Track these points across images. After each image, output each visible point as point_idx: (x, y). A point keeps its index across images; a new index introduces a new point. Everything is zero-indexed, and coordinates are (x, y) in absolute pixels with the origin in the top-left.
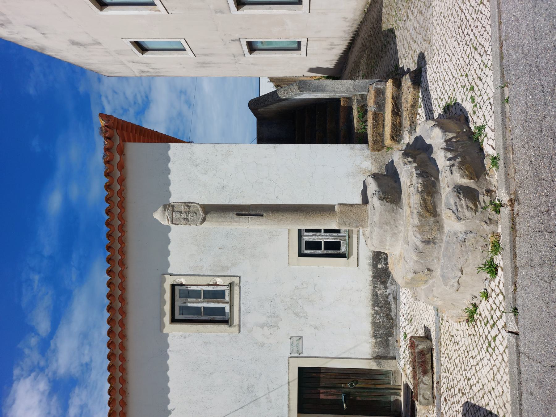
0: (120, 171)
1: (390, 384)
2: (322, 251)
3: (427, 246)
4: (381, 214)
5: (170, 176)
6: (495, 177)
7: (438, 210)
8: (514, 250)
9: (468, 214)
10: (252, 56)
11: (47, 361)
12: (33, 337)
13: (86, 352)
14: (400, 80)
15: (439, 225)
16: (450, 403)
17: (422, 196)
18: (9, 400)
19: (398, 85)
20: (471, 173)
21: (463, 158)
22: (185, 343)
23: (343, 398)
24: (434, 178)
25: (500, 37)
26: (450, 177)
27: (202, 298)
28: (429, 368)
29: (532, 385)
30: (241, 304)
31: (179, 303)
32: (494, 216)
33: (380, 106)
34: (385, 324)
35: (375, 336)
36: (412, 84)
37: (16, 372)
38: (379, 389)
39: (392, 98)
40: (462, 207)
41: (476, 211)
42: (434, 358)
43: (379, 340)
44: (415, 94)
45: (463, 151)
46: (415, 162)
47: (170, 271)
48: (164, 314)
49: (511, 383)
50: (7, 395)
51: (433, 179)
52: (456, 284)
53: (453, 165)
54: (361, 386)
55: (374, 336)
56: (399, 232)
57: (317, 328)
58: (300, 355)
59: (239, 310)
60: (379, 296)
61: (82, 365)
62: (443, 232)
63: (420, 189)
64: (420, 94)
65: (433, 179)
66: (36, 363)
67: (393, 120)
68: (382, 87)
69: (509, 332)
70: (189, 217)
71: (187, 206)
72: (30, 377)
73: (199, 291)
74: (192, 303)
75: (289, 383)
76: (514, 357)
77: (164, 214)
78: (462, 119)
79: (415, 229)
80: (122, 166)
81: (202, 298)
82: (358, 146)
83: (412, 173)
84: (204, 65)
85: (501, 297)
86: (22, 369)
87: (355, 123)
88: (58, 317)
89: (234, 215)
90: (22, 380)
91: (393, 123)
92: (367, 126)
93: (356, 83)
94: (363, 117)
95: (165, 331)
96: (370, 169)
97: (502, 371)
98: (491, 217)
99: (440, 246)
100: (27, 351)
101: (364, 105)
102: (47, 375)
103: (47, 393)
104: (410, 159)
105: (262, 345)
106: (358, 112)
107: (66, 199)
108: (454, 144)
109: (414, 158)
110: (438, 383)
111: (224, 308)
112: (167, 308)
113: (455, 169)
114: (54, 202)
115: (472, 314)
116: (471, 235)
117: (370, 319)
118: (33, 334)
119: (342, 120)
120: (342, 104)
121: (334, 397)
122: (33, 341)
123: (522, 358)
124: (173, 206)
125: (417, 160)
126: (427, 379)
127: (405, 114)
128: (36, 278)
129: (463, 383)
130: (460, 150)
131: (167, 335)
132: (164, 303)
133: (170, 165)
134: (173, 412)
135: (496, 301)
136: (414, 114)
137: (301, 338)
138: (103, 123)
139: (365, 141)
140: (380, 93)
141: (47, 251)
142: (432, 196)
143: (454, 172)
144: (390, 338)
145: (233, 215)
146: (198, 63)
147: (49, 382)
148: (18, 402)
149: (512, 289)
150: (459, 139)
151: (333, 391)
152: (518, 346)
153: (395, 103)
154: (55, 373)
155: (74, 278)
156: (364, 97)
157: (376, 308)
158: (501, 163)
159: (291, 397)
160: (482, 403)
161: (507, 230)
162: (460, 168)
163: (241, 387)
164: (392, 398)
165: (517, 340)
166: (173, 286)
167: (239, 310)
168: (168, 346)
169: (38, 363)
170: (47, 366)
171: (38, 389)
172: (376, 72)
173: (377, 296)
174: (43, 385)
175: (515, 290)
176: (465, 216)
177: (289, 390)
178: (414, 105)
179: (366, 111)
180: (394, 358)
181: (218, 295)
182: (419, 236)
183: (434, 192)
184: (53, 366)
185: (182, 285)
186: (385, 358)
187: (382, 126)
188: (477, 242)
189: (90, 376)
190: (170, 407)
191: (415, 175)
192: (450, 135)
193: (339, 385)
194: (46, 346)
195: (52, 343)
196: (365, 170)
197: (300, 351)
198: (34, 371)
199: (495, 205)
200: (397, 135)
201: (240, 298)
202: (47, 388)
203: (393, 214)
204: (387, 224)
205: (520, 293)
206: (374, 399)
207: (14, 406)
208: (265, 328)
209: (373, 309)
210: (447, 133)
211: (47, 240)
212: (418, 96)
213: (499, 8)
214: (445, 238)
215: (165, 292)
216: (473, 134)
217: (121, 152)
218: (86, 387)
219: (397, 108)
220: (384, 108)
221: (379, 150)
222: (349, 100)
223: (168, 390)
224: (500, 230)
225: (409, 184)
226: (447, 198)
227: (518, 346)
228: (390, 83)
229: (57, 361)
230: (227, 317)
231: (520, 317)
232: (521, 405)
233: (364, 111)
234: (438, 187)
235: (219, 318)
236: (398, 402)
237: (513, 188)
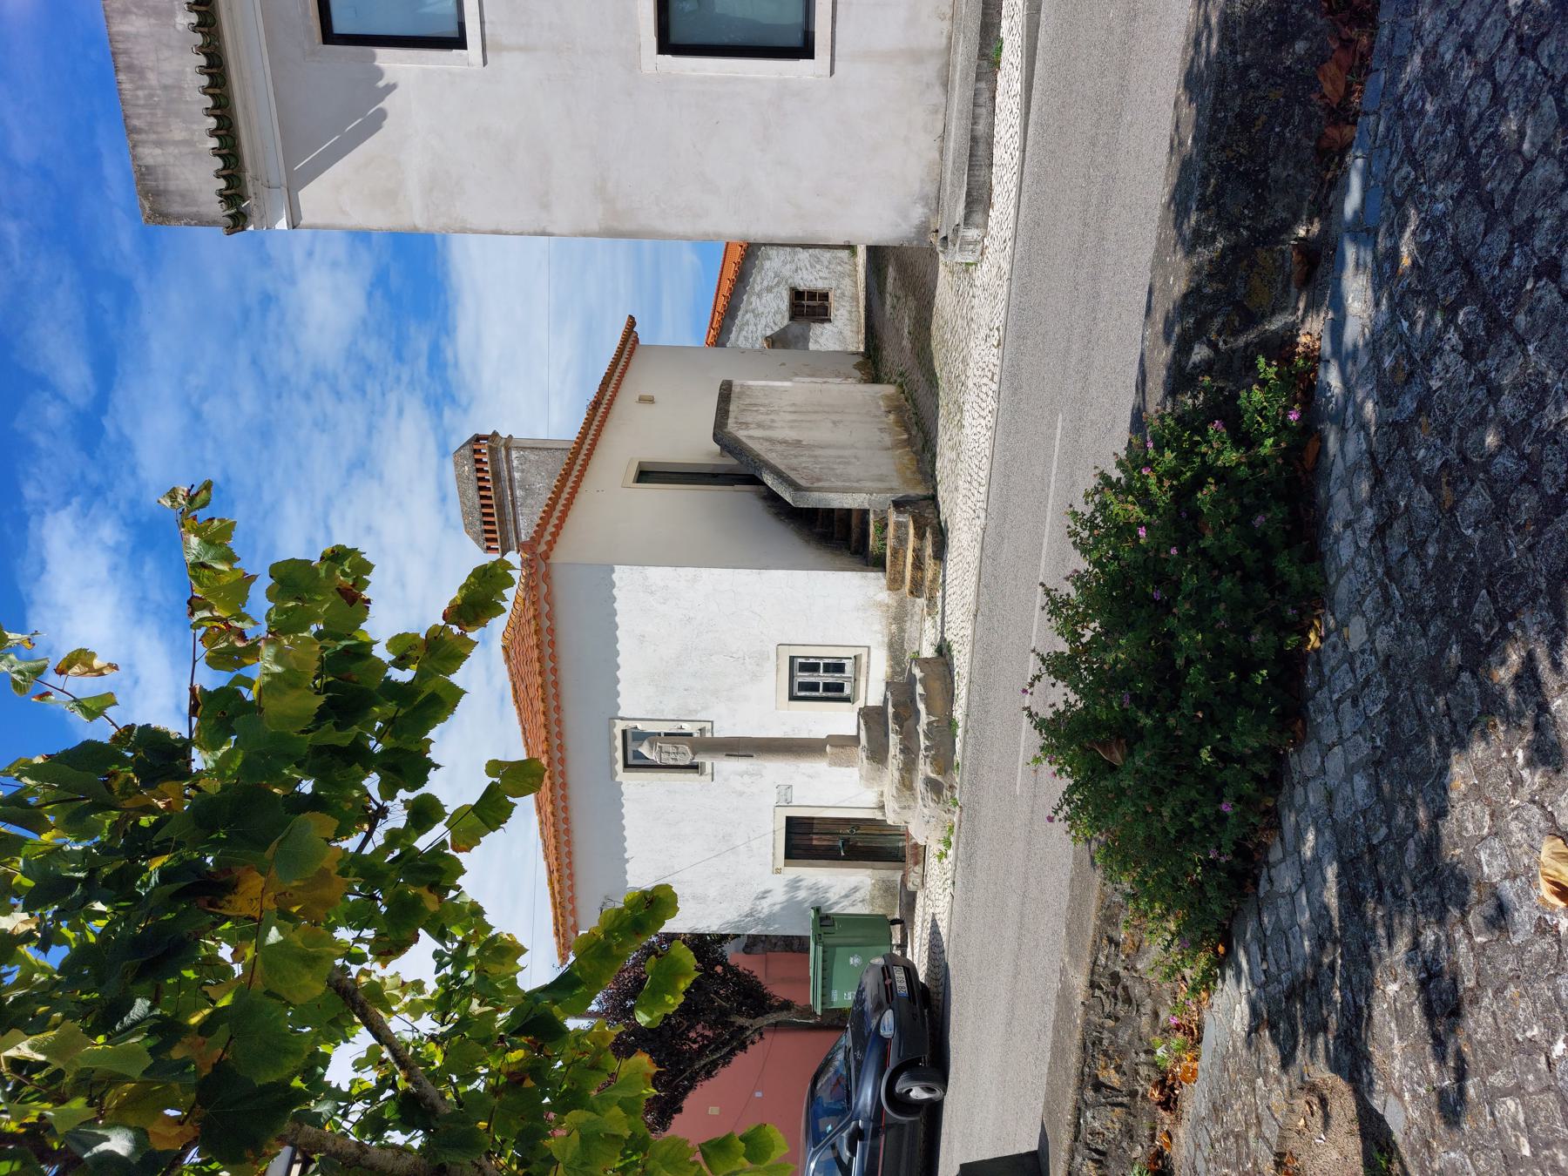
2: (821, 693)
26: (924, 769)
47: (620, 714)
72: (69, 509)
100: (41, 440)
102: (116, 507)
105: (741, 794)
112: (619, 755)
118: (47, 395)
126: (918, 869)
133: (615, 592)
137: (790, 787)
147: (126, 524)
154: (134, 504)
166: (624, 732)
169: (83, 477)
174: (109, 532)
190: (627, 856)
194: (90, 428)
195: (107, 422)
202: (123, 538)
207: (46, 578)
229: (133, 472)
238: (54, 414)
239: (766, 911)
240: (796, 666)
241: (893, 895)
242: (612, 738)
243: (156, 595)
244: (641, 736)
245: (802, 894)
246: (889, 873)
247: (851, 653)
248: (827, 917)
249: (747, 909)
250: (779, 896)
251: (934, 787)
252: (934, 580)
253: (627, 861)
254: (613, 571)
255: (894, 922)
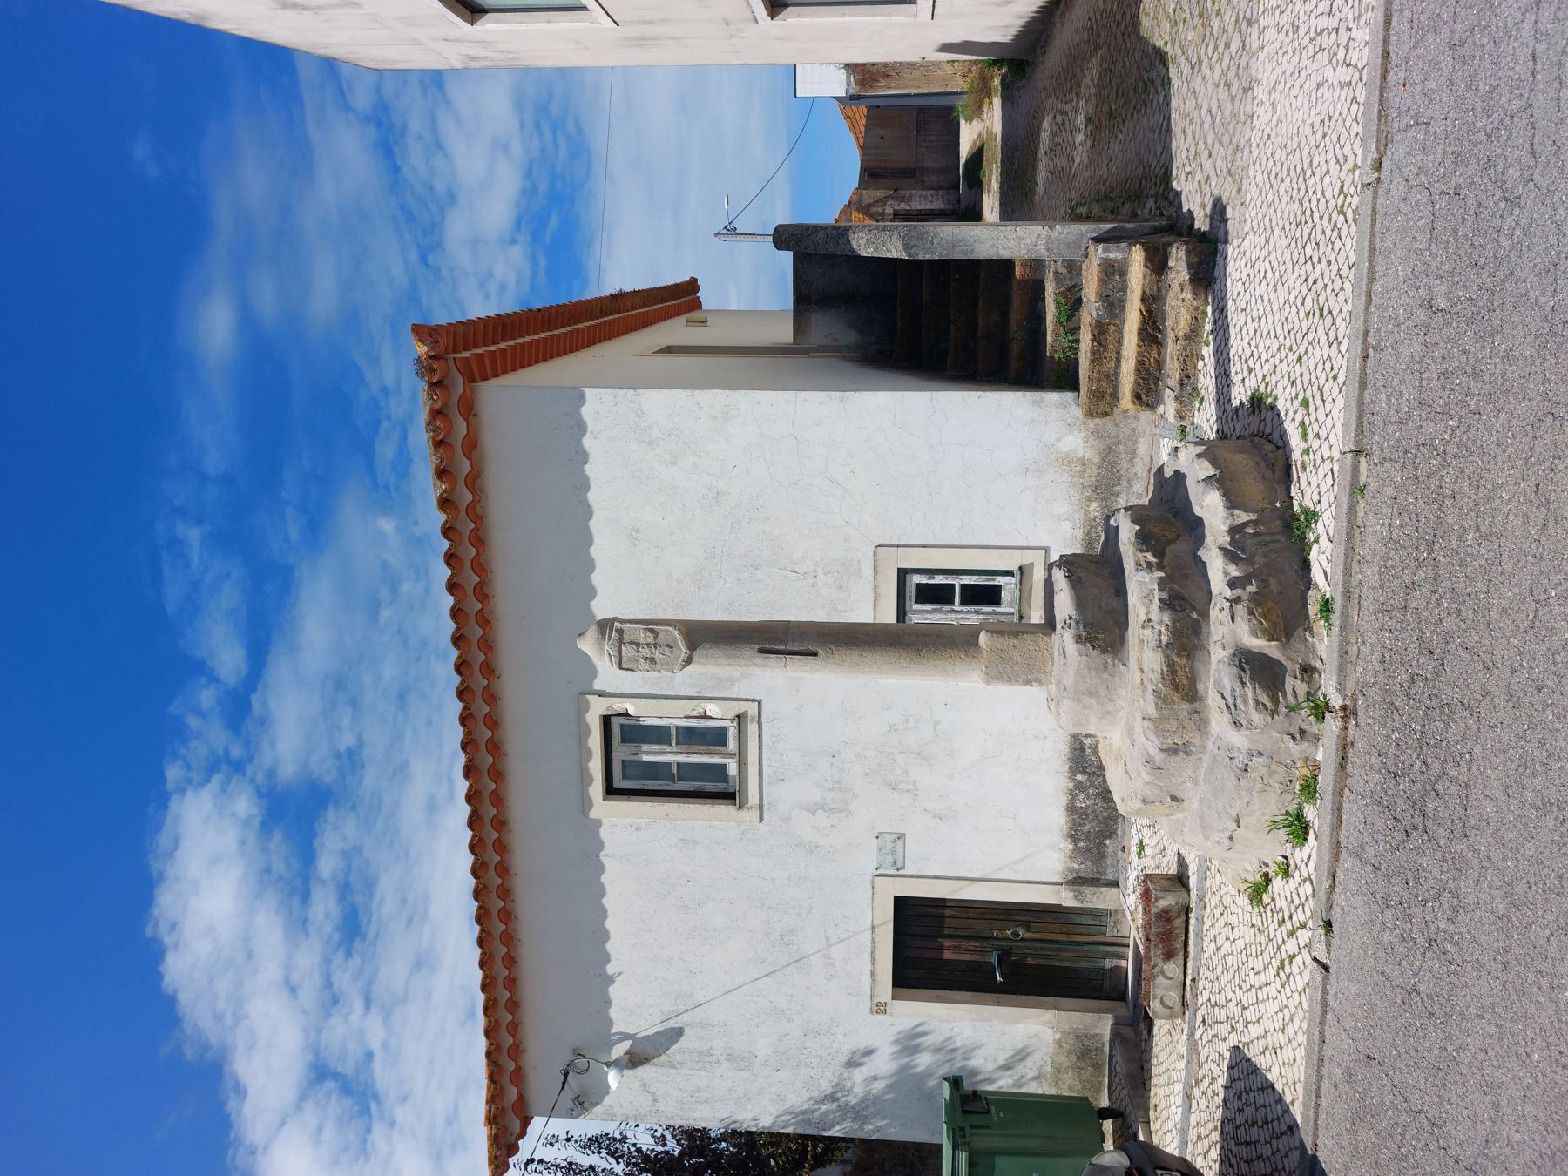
0: (469, 459)
1: (1104, 935)
3: (1172, 759)
4: (1078, 673)
5: (587, 467)
6: (1323, 643)
7: (1200, 687)
8: (1339, 810)
9: (1257, 717)
10: (777, 22)
11: (247, 744)
12: (205, 686)
13: (346, 722)
14: (1165, 251)
15: (1200, 720)
16: (1211, 1033)
17: (1167, 657)
18: (164, 840)
19: (1157, 264)
20: (1274, 624)
21: (1264, 583)
22: (632, 834)
23: (994, 959)
24: (1200, 614)
25: (1366, 333)
26: (1229, 630)
27: (674, 742)
28: (1180, 945)
29: (1338, 1071)
30: (765, 762)
31: (621, 753)
32: (1312, 726)
33: (1113, 304)
34: (1095, 825)
35: (1074, 837)
36: (1191, 280)
37: (173, 773)
38: (1078, 943)
39: (1143, 300)
40: (1245, 702)
41: (1274, 712)
42: (1191, 928)
43: (1081, 844)
44: (1197, 309)
45: (1266, 564)
46: (1160, 567)
47: (597, 685)
48: (591, 780)
49: (1309, 1054)
50: (159, 827)
51: (1195, 615)
52: (1226, 842)
53: (1237, 600)
54: (1038, 936)
55: (1072, 836)
56: (1118, 711)
57: (938, 816)
58: (899, 873)
59: (760, 773)
60: (1088, 751)
61: (338, 755)
62: (1207, 733)
63: (1164, 639)
64: (1209, 309)
65: (1195, 615)
66: (220, 751)
67: (1140, 354)
68: (1120, 256)
69: (1315, 959)
70: (657, 655)
71: (652, 631)
73: (668, 728)
74: (652, 754)
75: (873, 928)
76: (1317, 1010)
77: (601, 646)
78: (1280, 465)
79: (1146, 723)
80: (472, 445)
81: (674, 742)
82: (1052, 397)
83: (1151, 591)
84: (641, 42)
85: (1308, 888)
86: (188, 767)
87: (1049, 332)
88: (263, 633)
89: (754, 652)
90: (190, 793)
91: (1140, 363)
92: (1078, 341)
93: (1055, 234)
94: (1069, 318)
95: (593, 814)
96: (1080, 455)
97: (1297, 1021)
98: (1305, 727)
99: (1200, 759)
100: (193, 722)
101: (1075, 286)
102: (252, 780)
103: (256, 822)
104: (1151, 558)
105: (812, 849)
106: (1058, 306)
107: (246, 319)
108: (1249, 542)
109: (1160, 554)
110: (1193, 980)
111: (724, 767)
112: (596, 766)
113: (1241, 610)
114: (215, 327)
115: (1258, 891)
116: (1261, 760)
117: (1064, 800)
118: (204, 680)
119: (1016, 314)
120: (1018, 272)
121: (976, 957)
122: (207, 697)
123: (1329, 1016)
124: (620, 631)
125: (1166, 561)
126: (1172, 968)
127: (1172, 349)
128: (194, 535)
129: (1233, 1009)
130: (1260, 560)
131: (599, 823)
132: (589, 754)
133: (587, 442)
134: (618, 980)
135: (1301, 891)
136: (1189, 357)
137: (901, 837)
138: (422, 349)
139: (1075, 387)
140: (1113, 273)
141: (214, 462)
142: (1189, 657)
143: (1238, 619)
144: (1108, 842)
145: (750, 652)
146: (626, 39)
147: (260, 796)
148: (186, 844)
149: (1327, 884)
150: (1262, 529)
151: (972, 944)
152: (1325, 992)
153: (1149, 312)
154: (271, 773)
155: (294, 533)
156: (1073, 267)
157: (1079, 777)
158: (1335, 618)
159: (877, 956)
160: (1262, 1062)
161: (1334, 755)
162: (1251, 613)
163: (767, 934)
164: (1108, 964)
165: (1325, 980)
166: (606, 720)
167: (760, 773)
168: (601, 846)
169: (227, 751)
170: (251, 759)
171: (234, 814)
172: (1120, 136)
173: (1082, 749)
174: (244, 805)
175: (1333, 887)
176: (1250, 721)
177: (873, 942)
178: (1193, 335)
179: (1079, 301)
180: (1116, 884)
181: (717, 738)
182: (1154, 738)
183: (1195, 647)
184: (266, 758)
185: (626, 715)
186: (1095, 882)
187: (1114, 355)
188: (1271, 773)
189: (360, 782)
190: (611, 969)
191: (1156, 601)
192: (1243, 517)
193: (987, 933)
194: (239, 707)
195: (255, 700)
196: (1067, 455)
197: (899, 865)
198: (219, 770)
199: (1317, 706)
200: (1149, 390)
201: (760, 748)
202: (255, 811)
203: (1105, 675)
204: (1091, 695)
205: (1339, 898)
206: (1066, 964)
207: (179, 853)
208: (820, 813)
209: (1072, 778)
210: (1236, 512)
211: (211, 431)
212: (1205, 313)
213: (1371, 261)
214: (1210, 745)
215: (588, 732)
216: (1294, 517)
217: (469, 408)
218: (354, 808)
219: (1154, 322)
220: (1123, 309)
221: (1106, 414)
222: (1036, 265)
223: (605, 936)
224: (1320, 757)
225: (1143, 617)
226: (1218, 671)
227: (1325, 992)
228: (1137, 255)
230: (733, 785)
231: (1335, 942)
232: (1318, 1096)
233: (1072, 303)
234: (1204, 636)
235: (717, 789)
236: (1119, 973)
237: (1350, 685)
238: (207, 697)
239: (859, 1090)
240: (911, 592)
241: (1097, 1067)
242: (585, 731)
243: (279, 867)
244: (638, 733)
245: (924, 1060)
246: (1087, 1018)
247: (1010, 562)
248: (976, 1095)
249: (826, 1087)
250: (883, 1064)
251: (1260, 671)
252: (1193, 335)
253: (611, 980)
254: (582, 399)
255: (1104, 1114)
